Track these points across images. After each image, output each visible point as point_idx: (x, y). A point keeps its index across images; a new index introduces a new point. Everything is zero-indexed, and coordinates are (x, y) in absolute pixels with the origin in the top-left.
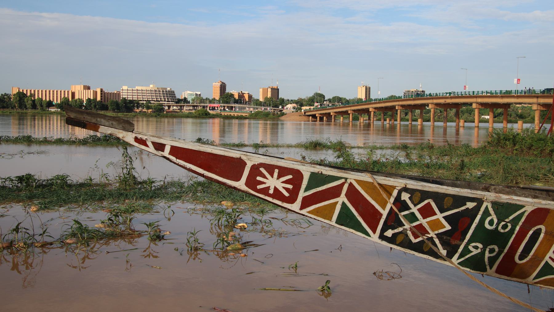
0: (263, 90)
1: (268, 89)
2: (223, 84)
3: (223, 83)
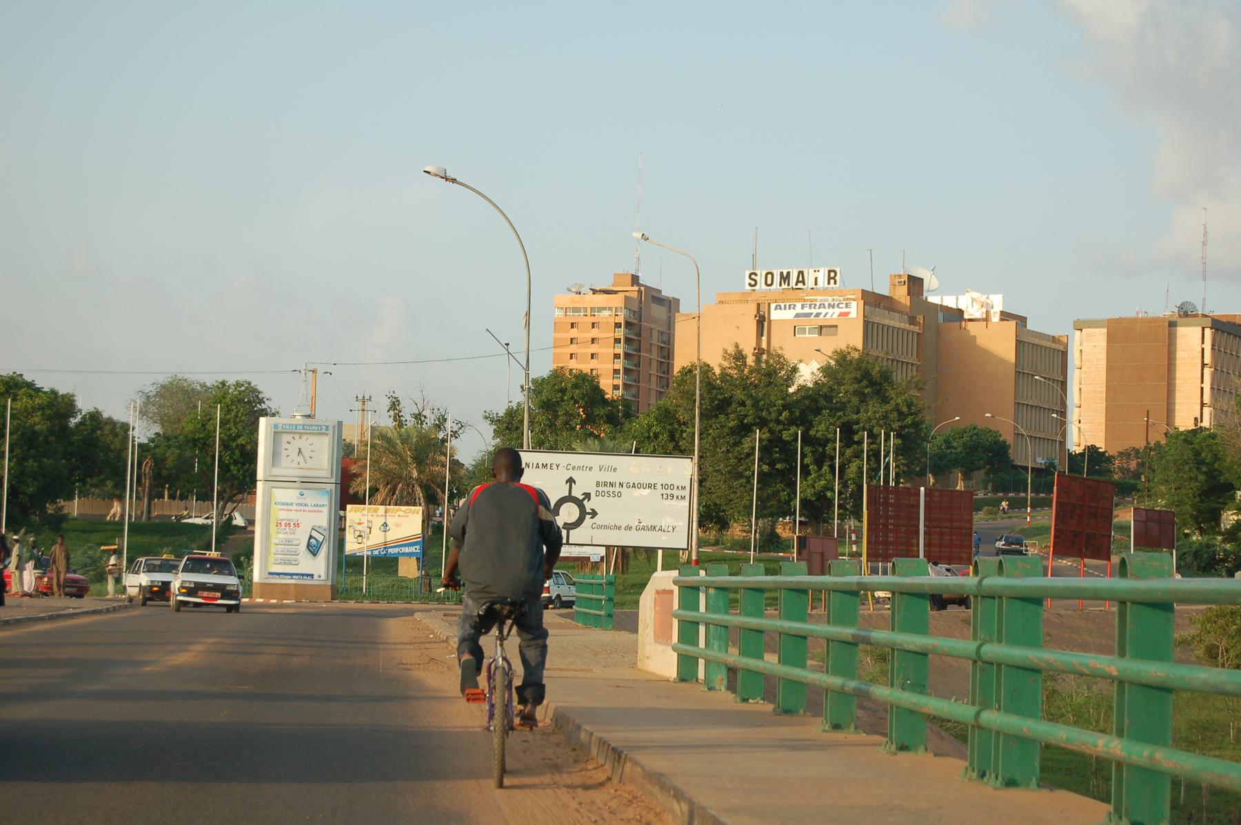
0: (1111, 339)
1: (1181, 331)
2: (658, 312)
3: (655, 297)
